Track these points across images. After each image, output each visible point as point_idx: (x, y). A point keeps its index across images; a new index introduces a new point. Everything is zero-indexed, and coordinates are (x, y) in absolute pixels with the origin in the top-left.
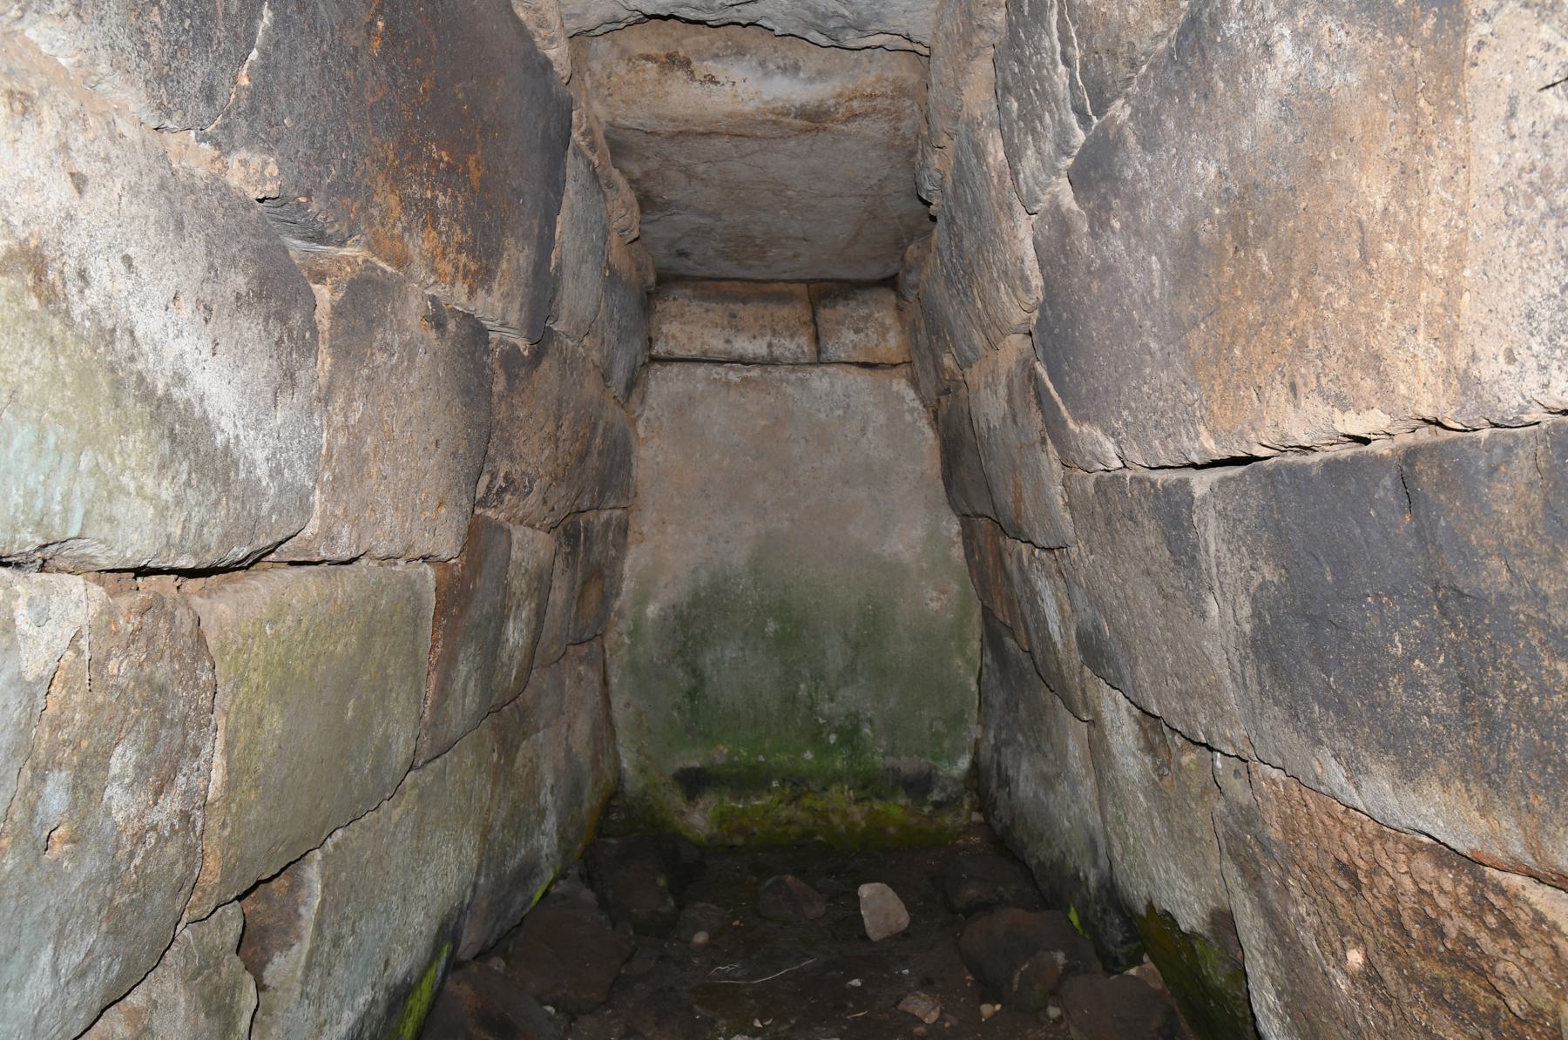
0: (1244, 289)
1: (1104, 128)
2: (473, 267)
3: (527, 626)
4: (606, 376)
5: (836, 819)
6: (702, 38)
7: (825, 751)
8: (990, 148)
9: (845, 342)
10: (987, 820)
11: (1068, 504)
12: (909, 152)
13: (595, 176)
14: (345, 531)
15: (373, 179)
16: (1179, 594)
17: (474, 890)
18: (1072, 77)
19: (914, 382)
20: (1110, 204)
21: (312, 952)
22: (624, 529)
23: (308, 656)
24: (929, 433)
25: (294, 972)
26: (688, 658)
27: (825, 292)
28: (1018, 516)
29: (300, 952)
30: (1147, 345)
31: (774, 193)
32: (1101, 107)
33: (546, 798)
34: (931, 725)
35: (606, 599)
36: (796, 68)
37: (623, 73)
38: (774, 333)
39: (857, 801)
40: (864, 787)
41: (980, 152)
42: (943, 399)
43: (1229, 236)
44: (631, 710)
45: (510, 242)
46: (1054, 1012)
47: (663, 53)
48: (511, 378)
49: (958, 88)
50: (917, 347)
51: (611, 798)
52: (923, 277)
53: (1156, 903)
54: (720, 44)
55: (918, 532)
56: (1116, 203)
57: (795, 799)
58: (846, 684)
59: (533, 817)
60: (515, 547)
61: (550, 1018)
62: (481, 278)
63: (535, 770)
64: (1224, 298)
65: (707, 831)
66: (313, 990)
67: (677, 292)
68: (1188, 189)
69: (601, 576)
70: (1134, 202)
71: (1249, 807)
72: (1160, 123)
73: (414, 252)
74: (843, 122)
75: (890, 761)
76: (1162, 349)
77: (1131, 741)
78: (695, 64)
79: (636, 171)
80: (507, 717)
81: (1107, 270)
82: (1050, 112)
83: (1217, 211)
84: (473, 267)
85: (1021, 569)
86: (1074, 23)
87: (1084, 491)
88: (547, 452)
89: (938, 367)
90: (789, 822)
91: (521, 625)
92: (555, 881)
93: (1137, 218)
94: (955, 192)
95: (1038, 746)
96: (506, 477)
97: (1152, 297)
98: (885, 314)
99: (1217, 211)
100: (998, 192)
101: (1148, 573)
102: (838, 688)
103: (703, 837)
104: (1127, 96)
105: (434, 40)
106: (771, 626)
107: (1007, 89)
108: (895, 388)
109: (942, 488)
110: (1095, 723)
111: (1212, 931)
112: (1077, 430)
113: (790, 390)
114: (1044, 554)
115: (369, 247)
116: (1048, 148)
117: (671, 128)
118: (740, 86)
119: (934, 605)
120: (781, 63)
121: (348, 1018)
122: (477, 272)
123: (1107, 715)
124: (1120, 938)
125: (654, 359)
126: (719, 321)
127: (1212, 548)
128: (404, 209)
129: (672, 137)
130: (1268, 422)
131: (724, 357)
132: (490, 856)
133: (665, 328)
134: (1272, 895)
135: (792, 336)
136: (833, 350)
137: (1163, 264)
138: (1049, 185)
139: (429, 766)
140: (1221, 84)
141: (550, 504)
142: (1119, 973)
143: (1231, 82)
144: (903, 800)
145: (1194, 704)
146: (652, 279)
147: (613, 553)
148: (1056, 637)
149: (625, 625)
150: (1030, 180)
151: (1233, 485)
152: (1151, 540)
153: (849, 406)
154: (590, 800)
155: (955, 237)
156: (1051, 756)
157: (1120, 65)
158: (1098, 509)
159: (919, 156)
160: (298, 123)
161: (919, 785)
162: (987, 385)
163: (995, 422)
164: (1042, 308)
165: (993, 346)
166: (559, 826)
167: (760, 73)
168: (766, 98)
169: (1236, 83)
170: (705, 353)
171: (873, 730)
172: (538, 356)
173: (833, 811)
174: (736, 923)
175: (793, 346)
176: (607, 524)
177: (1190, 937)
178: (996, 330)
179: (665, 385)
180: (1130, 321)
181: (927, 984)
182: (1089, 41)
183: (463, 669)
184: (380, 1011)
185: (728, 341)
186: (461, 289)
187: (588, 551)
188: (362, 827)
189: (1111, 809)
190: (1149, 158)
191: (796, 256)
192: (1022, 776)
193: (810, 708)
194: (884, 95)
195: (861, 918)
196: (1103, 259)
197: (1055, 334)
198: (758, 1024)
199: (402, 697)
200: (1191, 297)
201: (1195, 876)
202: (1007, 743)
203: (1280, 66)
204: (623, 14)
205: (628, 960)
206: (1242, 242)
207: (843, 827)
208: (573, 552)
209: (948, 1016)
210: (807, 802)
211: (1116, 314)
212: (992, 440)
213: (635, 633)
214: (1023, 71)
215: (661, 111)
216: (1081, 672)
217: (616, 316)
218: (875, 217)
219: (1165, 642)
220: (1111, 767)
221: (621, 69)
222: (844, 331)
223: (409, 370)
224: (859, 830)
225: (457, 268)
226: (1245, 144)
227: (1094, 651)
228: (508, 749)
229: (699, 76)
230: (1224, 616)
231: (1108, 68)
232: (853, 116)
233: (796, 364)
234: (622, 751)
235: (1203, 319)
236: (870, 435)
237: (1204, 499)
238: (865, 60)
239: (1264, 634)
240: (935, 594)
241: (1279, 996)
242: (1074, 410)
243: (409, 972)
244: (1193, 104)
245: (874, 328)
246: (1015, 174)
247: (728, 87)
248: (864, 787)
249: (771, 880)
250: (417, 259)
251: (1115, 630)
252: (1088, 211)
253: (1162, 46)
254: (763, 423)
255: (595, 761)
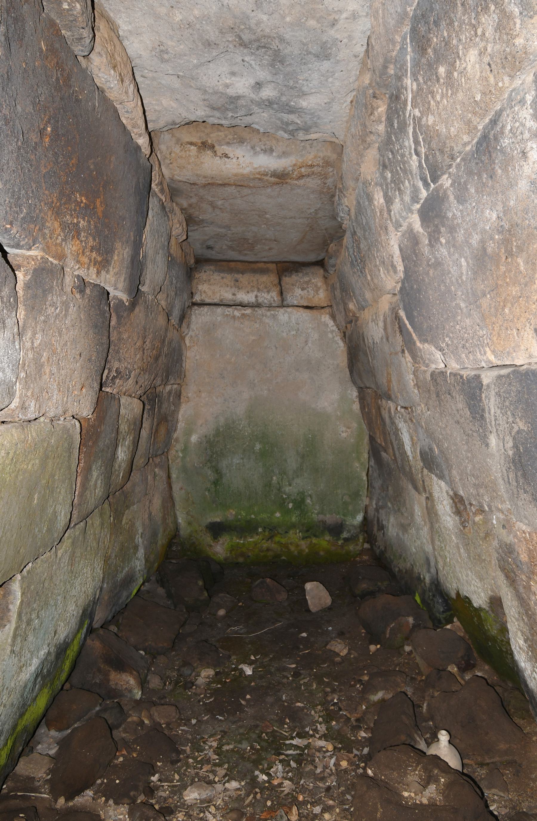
0: (510, 278)
1: (436, 190)
2: (99, 259)
3: (129, 449)
4: (168, 316)
5: (292, 548)
6: (220, 134)
7: (287, 512)
8: (376, 196)
9: (297, 295)
10: (372, 547)
11: (417, 385)
12: (331, 195)
13: (163, 207)
14: (32, 404)
15: (46, 214)
16: (475, 434)
17: (101, 591)
18: (420, 162)
19: (333, 317)
20: (439, 230)
21: (16, 629)
22: (179, 395)
23: (13, 472)
24: (341, 344)
25: (7, 640)
26: (214, 464)
27: (286, 268)
28: (389, 390)
29: (10, 629)
30: (459, 304)
31: (259, 216)
32: (435, 179)
33: (139, 540)
34: (342, 498)
35: (169, 433)
36: (271, 150)
37: (178, 151)
38: (259, 290)
39: (303, 538)
40: (307, 531)
41: (370, 199)
42: (349, 326)
43: (503, 250)
44: (183, 491)
45: (118, 245)
46: (407, 648)
47: (199, 141)
48: (119, 317)
49: (358, 164)
50: (335, 298)
51: (172, 539)
52: (338, 262)
53: (461, 592)
54: (231, 137)
55: (335, 397)
56: (443, 229)
57: (271, 538)
58: (298, 476)
59: (132, 551)
60: (122, 407)
61: (142, 657)
62: (103, 265)
63: (133, 525)
64: (500, 282)
65: (224, 555)
66: (17, 649)
67: (206, 268)
68: (481, 225)
69: (167, 421)
70: (452, 230)
71: (510, 544)
72: (467, 189)
73: (67, 252)
74: (297, 179)
75: (321, 517)
76: (467, 307)
77: (448, 509)
78: (217, 148)
79: (185, 204)
80: (117, 499)
81: (438, 264)
82: (408, 180)
83: (497, 237)
84: (99, 259)
85: (390, 417)
86: (422, 134)
87: (425, 378)
88: (138, 356)
89: (346, 309)
90: (268, 550)
91: (125, 449)
92: (143, 584)
93: (454, 238)
94: (356, 218)
95: (399, 509)
96: (116, 371)
97: (462, 280)
98: (318, 281)
99: (497, 237)
100: (380, 220)
101: (458, 422)
102: (293, 479)
103: (222, 558)
104: (449, 173)
105: (78, 137)
106: (258, 447)
107: (385, 166)
108: (323, 319)
109: (348, 373)
110: (430, 498)
111: (490, 607)
112: (421, 347)
113: (267, 321)
114: (403, 410)
115: (43, 250)
116: (407, 198)
117: (203, 181)
118: (241, 160)
119: (344, 435)
120: (263, 148)
121: (36, 662)
122: (101, 262)
123: (436, 495)
124: (442, 610)
125: (194, 304)
126: (229, 283)
127: (492, 411)
128: (63, 230)
129: (205, 186)
130: (522, 348)
131: (232, 303)
132: (109, 572)
133: (200, 287)
134: (521, 590)
135: (268, 292)
136: (290, 299)
137: (468, 263)
138: (407, 218)
139: (77, 526)
140: (500, 171)
141: (140, 384)
142: (442, 628)
143: (505, 170)
144: (328, 537)
145: (481, 491)
146: (192, 261)
147: (173, 408)
148: (409, 453)
149: (179, 446)
150: (397, 215)
151: (504, 379)
152: (460, 406)
153: (298, 330)
154: (162, 540)
155: (357, 242)
156: (406, 514)
157: (446, 157)
158: (432, 388)
159: (337, 197)
160: (5, 185)
161: (336, 530)
162: (373, 321)
163: (377, 340)
164: (403, 282)
165: (376, 301)
166: (145, 555)
167: (252, 153)
168: (255, 166)
169: (507, 171)
170: (221, 301)
171: (311, 501)
172: (133, 304)
173: (291, 544)
174: (240, 604)
175: (269, 297)
176: (170, 393)
177: (480, 609)
178: (378, 290)
179: (200, 318)
180: (450, 291)
181: (341, 634)
182: (429, 144)
183: (95, 474)
184: (52, 657)
185: (234, 294)
186: (93, 271)
187: (160, 408)
188: (42, 561)
189: (437, 543)
190: (461, 207)
191: (270, 249)
192: (390, 524)
193: (279, 490)
194: (318, 165)
195: (306, 600)
196: (436, 258)
197: (411, 295)
198: (253, 658)
199: (63, 491)
200: (483, 281)
201: (481, 579)
202: (382, 507)
203: (531, 163)
204: (178, 121)
205: (183, 626)
206: (510, 254)
207: (296, 553)
208: (153, 409)
209: (353, 652)
210: (277, 539)
211: (443, 288)
212: (375, 349)
213: (185, 450)
214: (394, 157)
215: (199, 172)
216: (422, 472)
217: (174, 282)
218: (313, 229)
219: (467, 458)
220: (438, 521)
221: (177, 149)
222: (296, 289)
223: (66, 316)
224: (305, 553)
225: (90, 260)
226: (512, 203)
227: (429, 461)
228: (118, 515)
229: (219, 154)
230: (498, 446)
231: (439, 159)
232: (301, 177)
233: (270, 307)
234: (178, 513)
235: (489, 293)
236: (310, 345)
237: (488, 386)
238: (308, 146)
239: (520, 456)
240: (344, 429)
241: (525, 641)
242: (420, 336)
243: (67, 636)
244: (484, 180)
245: (310, 288)
246: (389, 211)
247: (234, 160)
248: (307, 531)
249: (258, 581)
250: (69, 256)
251: (442, 452)
252: (428, 233)
253: (468, 148)
254: (253, 338)
255: (164, 519)
